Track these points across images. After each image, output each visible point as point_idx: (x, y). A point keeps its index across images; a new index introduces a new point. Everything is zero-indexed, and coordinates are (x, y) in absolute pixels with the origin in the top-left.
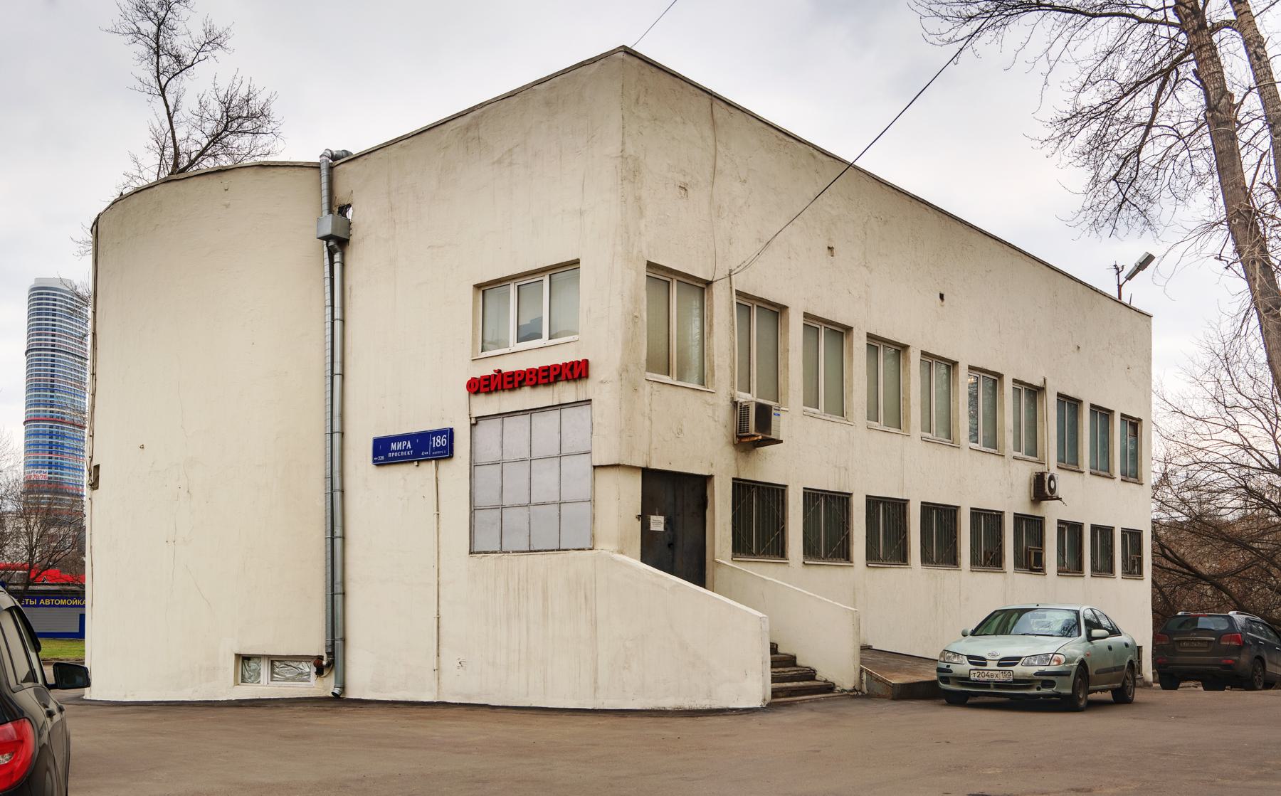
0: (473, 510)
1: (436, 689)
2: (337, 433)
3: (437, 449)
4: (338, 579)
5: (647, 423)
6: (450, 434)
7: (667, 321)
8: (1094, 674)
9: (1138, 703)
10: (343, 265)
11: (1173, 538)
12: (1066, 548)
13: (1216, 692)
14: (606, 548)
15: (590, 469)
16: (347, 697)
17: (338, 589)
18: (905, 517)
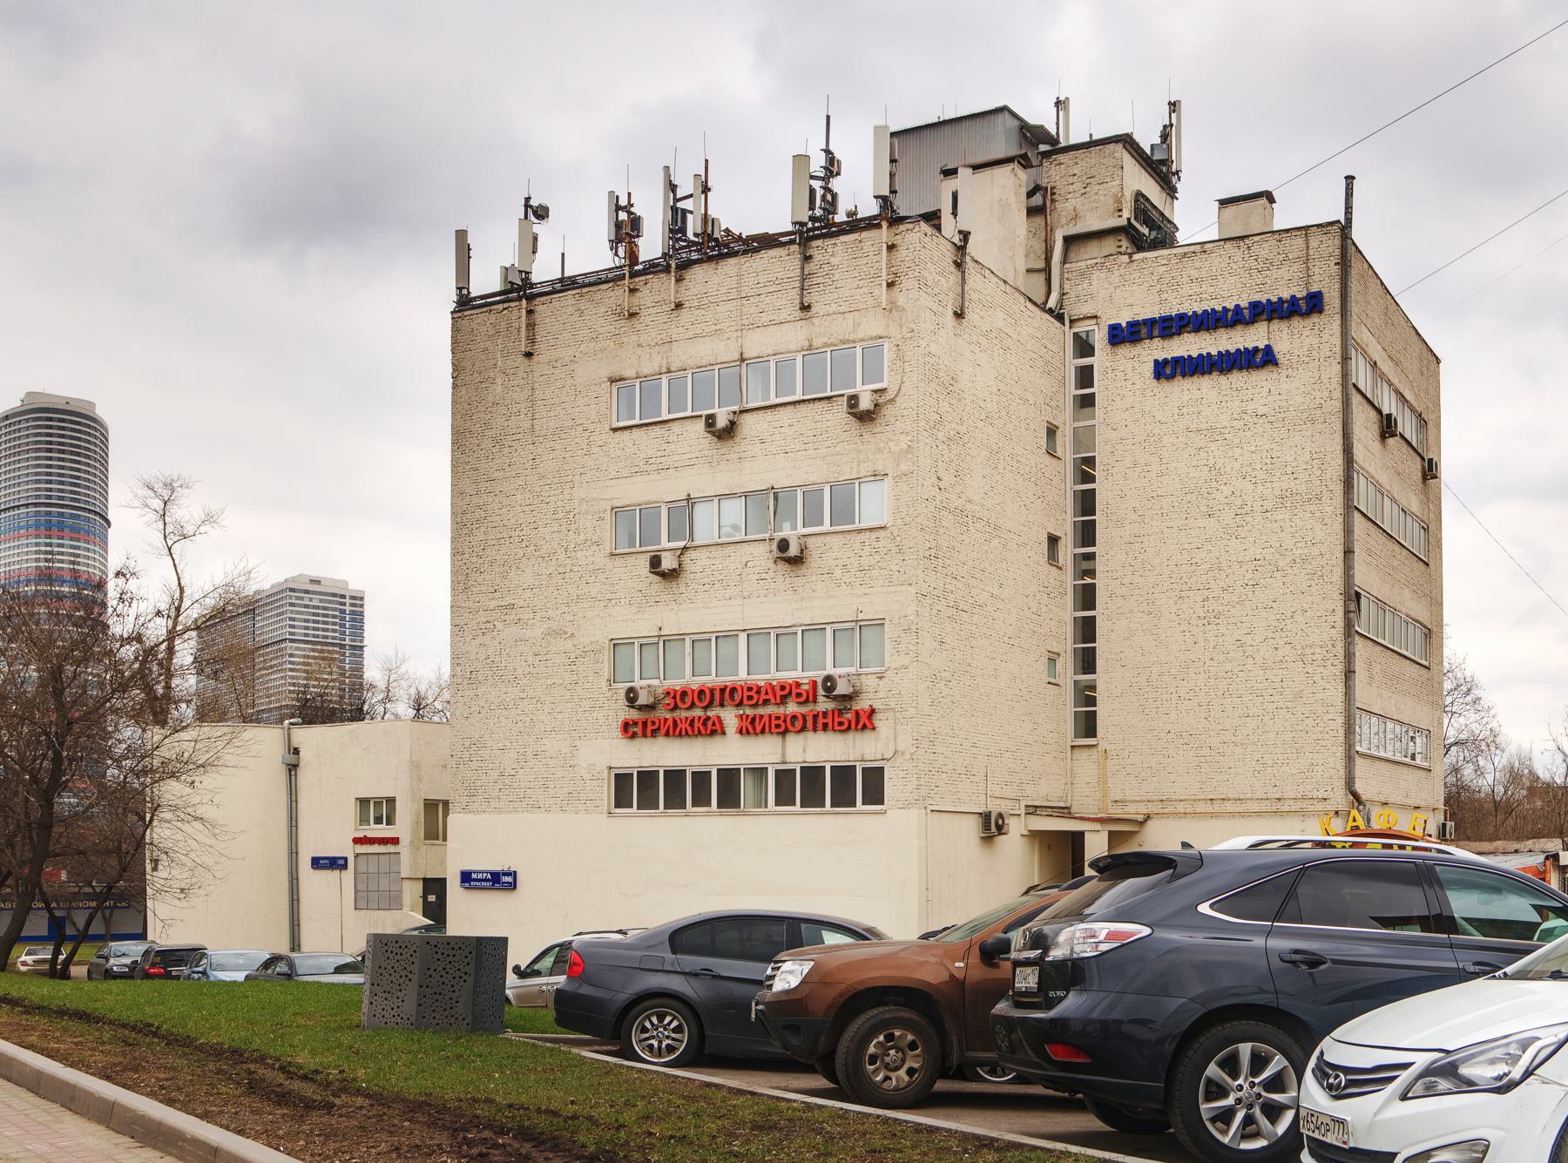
0: (356, 892)
2: (293, 852)
3: (505, 883)
4: (296, 918)
5: (425, 861)
6: (346, 859)
10: (296, 776)
14: (406, 909)
16: (448, 934)
17: (296, 923)
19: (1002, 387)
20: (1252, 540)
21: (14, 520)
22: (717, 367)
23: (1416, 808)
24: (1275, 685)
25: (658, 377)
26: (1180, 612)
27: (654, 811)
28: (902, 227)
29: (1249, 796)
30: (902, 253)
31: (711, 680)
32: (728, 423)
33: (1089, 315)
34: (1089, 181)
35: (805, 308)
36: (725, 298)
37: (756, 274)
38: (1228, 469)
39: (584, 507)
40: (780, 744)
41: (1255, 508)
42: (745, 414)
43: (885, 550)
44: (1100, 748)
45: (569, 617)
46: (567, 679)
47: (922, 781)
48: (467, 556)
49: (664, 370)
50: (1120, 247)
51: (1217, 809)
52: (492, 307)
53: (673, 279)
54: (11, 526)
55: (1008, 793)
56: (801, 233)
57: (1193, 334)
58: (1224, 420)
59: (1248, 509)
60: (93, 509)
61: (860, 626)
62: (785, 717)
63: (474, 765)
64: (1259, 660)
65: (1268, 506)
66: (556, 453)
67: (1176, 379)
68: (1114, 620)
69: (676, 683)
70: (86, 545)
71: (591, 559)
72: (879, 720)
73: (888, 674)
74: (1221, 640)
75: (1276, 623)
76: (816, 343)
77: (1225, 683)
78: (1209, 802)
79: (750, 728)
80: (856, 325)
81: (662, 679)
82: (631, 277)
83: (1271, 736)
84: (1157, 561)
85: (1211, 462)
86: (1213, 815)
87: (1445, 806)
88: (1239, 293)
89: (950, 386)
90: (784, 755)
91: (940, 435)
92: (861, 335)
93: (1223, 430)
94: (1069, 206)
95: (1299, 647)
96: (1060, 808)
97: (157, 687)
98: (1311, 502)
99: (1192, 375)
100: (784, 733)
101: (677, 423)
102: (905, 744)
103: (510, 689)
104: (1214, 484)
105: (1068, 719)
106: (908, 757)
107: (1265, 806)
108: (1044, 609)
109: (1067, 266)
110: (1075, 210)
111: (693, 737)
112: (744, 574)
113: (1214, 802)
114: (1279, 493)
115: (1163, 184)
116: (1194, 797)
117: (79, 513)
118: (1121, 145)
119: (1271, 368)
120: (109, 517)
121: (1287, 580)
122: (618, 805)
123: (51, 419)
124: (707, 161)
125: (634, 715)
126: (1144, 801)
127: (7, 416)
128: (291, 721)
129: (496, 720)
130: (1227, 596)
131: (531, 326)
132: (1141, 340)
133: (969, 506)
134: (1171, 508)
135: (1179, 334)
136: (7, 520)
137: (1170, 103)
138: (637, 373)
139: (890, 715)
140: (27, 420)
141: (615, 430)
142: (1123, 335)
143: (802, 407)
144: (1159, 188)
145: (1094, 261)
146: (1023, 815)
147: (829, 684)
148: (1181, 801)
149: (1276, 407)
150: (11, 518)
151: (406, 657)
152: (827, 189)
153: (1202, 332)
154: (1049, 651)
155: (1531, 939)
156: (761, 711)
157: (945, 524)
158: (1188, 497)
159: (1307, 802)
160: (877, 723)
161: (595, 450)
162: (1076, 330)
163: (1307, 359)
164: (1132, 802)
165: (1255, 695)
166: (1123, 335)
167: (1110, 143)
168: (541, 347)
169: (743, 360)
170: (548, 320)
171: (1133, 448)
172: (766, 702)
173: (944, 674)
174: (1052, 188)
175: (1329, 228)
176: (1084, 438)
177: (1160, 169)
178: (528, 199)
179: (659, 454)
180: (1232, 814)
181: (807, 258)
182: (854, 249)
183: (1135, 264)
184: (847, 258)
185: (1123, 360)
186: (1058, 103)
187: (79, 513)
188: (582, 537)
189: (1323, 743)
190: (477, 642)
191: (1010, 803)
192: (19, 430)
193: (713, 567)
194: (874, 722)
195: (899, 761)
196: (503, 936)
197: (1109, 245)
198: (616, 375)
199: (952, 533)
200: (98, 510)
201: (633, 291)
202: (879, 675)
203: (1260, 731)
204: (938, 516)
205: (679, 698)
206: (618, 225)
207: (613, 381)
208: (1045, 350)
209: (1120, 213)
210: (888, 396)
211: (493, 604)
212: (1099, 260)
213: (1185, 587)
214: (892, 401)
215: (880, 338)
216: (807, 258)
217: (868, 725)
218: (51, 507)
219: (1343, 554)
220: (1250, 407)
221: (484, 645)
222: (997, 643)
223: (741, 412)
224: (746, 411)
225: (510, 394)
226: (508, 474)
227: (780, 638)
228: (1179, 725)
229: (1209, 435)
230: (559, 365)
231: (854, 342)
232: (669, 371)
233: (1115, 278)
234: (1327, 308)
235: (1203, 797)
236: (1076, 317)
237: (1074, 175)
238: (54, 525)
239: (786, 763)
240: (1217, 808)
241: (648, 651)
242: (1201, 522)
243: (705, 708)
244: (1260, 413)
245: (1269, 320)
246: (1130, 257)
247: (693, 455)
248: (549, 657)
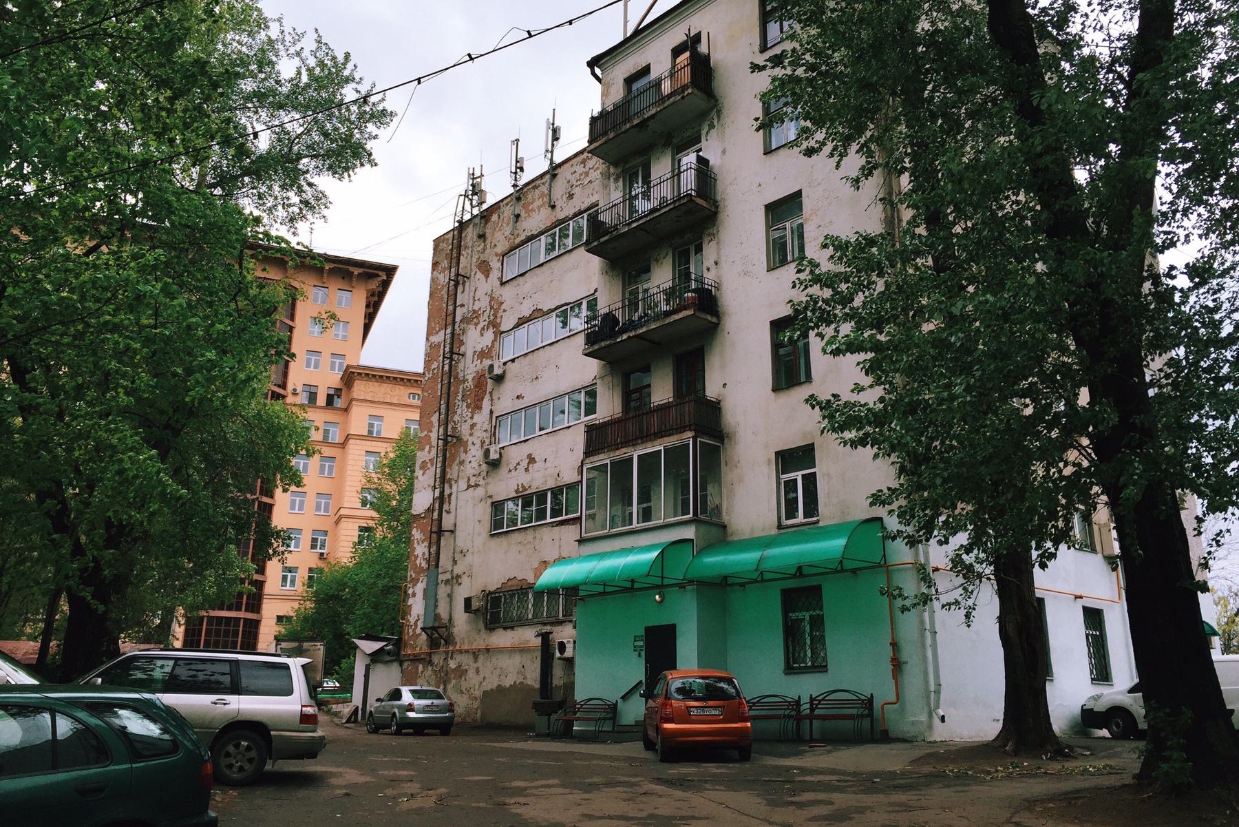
1: (518, 241)
8: (677, 684)
9: (733, 542)
11: (814, 74)
12: (283, 733)
13: (656, 624)
15: (458, 533)
18: (1105, 659)
90: (798, 725)
97: (1229, 358)
147: (330, 684)
151: (341, 58)
155: (546, 519)
177: (1186, 358)
196: (588, 123)
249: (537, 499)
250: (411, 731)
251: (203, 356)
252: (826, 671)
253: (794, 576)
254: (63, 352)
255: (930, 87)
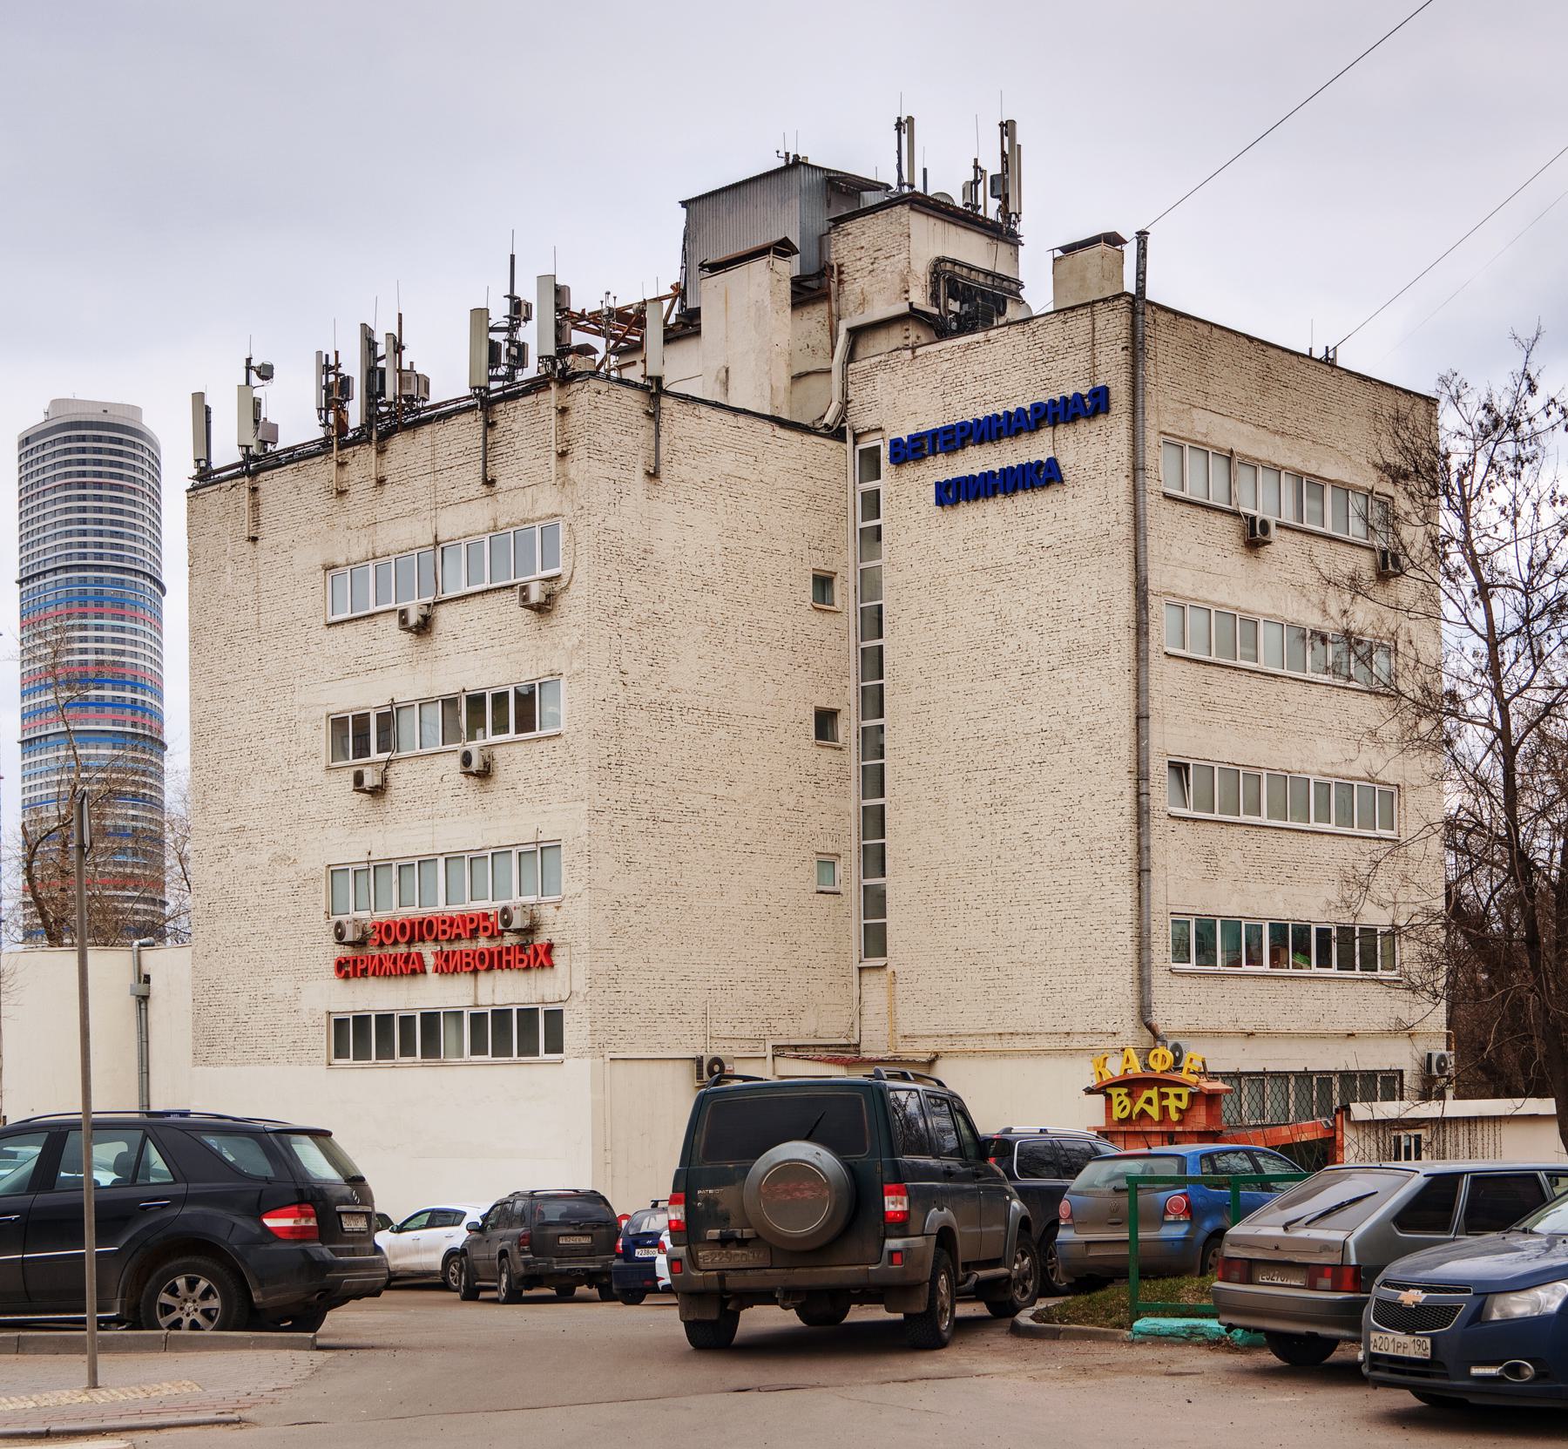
7: (1180, 472)
10: (146, 1009)
19: (732, 544)
20: (1038, 705)
21: (40, 593)
22: (416, 552)
23: (1349, 1035)
24: (1063, 889)
25: (364, 564)
26: (967, 798)
27: (367, 1062)
28: (574, 387)
29: (1037, 1029)
30: (573, 417)
31: (413, 912)
32: (420, 619)
33: (874, 427)
34: (876, 255)
35: (489, 482)
36: (422, 472)
37: (447, 444)
38: (1014, 616)
39: (303, 715)
40: (473, 983)
41: (1041, 666)
42: (440, 606)
43: (560, 760)
44: (889, 970)
45: (291, 841)
46: (291, 912)
47: (598, 1026)
48: (204, 771)
49: (370, 556)
50: (907, 338)
51: (1006, 1047)
52: (222, 485)
53: (374, 451)
54: (36, 603)
55: (746, 1031)
56: (483, 399)
57: (977, 447)
58: (1010, 555)
59: (1034, 666)
60: (142, 569)
61: (542, 848)
62: (474, 954)
63: (213, 1010)
64: (1046, 858)
65: (1055, 661)
66: (279, 651)
67: (960, 505)
68: (902, 810)
69: (383, 916)
70: (133, 625)
71: (310, 773)
72: (558, 956)
73: (564, 904)
74: (1008, 831)
75: (1062, 811)
76: (501, 524)
77: (1012, 887)
78: (998, 1037)
79: (448, 966)
80: (534, 502)
81: (373, 908)
82: (340, 449)
83: (1059, 953)
84: (944, 734)
85: (997, 608)
86: (1003, 1054)
87: (1448, 1028)
88: (1024, 392)
89: (642, 561)
90: (476, 997)
91: (625, 622)
92: (538, 514)
93: (1008, 568)
94: (856, 288)
95: (1086, 841)
96: (841, 1046)
98: (1098, 656)
99: (976, 499)
100: (475, 972)
101: (382, 617)
102: (580, 984)
103: (242, 923)
104: (1000, 637)
105: (854, 935)
106: (582, 998)
107: (1054, 1043)
108: (808, 802)
109: (851, 366)
110: (862, 292)
111: (449, 975)
112: (441, 790)
113: (1003, 1037)
114: (1065, 645)
115: (990, 233)
116: (983, 1031)
117: (122, 576)
118: (907, 207)
119: (1056, 486)
120: (164, 581)
121: (1075, 755)
122: (337, 1056)
123: (83, 438)
124: (400, 315)
125: (347, 952)
126: (933, 1036)
127: (27, 439)
128: (142, 941)
129: (231, 958)
130: (1013, 777)
131: (255, 506)
132: (924, 456)
133: (673, 697)
134: (957, 667)
135: (963, 447)
136: (30, 593)
137: (1002, 125)
138: (347, 559)
139: (565, 950)
140: (53, 443)
141: (329, 625)
142: (909, 451)
143: (490, 598)
144: (987, 240)
145: (877, 359)
146: (770, 1058)
148: (970, 1035)
149: (1062, 537)
150: (36, 591)
152: (512, 342)
153: (987, 444)
154: (818, 853)
156: (457, 946)
157: (631, 724)
158: (974, 654)
159: (1095, 1037)
160: (555, 960)
161: (313, 648)
162: (861, 446)
163: (1093, 473)
164: (921, 1036)
165: (1043, 902)
166: (909, 451)
167: (896, 205)
168: (264, 530)
169: (437, 543)
170: (270, 498)
171: (919, 593)
172: (458, 937)
173: (633, 900)
174: (840, 266)
175: (1116, 303)
176: (870, 583)
178: (249, 360)
179: (367, 652)
180: (1022, 1053)
181: (490, 425)
182: (533, 413)
183: (918, 360)
184: (525, 424)
185: (908, 484)
186: (899, 125)
187: (122, 576)
188: (302, 749)
189: (1111, 962)
190: (212, 870)
191: (747, 1045)
192: (44, 470)
193: (414, 782)
194: (553, 958)
195: (574, 1002)
197: (895, 337)
198: (329, 562)
199: (646, 733)
200: (147, 570)
201: (342, 465)
202: (557, 905)
203: (1047, 948)
204: (621, 717)
205: (387, 931)
206: (328, 388)
207: (327, 568)
208: (810, 482)
209: (907, 296)
210: (563, 584)
211: (228, 825)
212: (883, 358)
213: (972, 767)
214: (566, 588)
215: (556, 516)
216: (490, 425)
217: (545, 963)
218: (101, 571)
219: (1134, 721)
220: (1037, 535)
221: (220, 873)
222: (725, 853)
223: (436, 604)
224: (441, 602)
225: (239, 585)
226: (238, 677)
227: (474, 861)
228: (967, 941)
229: (994, 575)
230: (279, 551)
231: (533, 521)
232: (375, 558)
233: (899, 380)
234: (1113, 406)
235: (991, 1031)
236: (861, 430)
237: (862, 248)
238: (91, 598)
239: (478, 1006)
240: (1005, 1044)
241: (362, 877)
242: (988, 685)
243: (410, 943)
244: (1046, 544)
245: (1054, 424)
246: (913, 353)
247: (395, 654)
248: (275, 887)
249: (1450, 1206)
250: (551, 1292)
251: (1230, 1328)
252: (340, 1052)
253: (1112, 1219)
254: (1470, 861)
255: (137, 918)
